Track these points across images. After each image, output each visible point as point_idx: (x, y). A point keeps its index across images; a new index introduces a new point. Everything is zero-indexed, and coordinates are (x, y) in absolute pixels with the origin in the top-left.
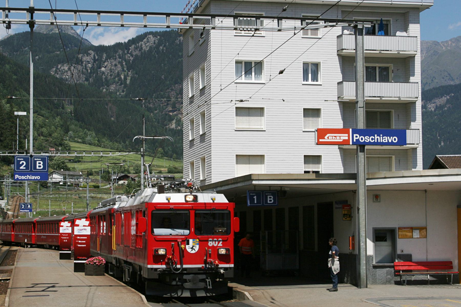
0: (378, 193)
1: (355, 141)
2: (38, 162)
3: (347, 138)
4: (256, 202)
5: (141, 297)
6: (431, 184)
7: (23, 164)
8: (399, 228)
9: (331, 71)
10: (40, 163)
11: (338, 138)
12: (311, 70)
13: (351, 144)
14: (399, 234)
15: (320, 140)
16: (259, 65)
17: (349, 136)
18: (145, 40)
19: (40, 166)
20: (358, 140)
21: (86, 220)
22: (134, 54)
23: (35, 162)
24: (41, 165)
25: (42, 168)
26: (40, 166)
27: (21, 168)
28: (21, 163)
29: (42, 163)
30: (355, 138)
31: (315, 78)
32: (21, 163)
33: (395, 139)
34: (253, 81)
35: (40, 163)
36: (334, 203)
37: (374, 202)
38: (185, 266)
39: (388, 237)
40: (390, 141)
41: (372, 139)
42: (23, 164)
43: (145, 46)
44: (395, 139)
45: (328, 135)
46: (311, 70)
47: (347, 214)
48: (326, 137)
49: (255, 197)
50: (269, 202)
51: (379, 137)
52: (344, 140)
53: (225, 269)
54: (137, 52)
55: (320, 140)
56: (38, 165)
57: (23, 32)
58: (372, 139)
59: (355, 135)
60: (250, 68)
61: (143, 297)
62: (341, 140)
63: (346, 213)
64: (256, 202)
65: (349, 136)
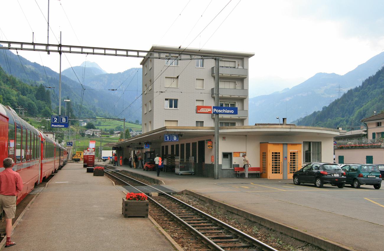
0: (225, 136)
1: (214, 112)
2: (63, 119)
3: (210, 110)
7: (56, 119)
8: (234, 152)
23: (62, 119)
24: (65, 120)
26: (64, 121)
27: (55, 121)
28: (55, 119)
29: (65, 119)
30: (214, 111)
32: (55, 119)
33: (232, 112)
35: (64, 119)
37: (223, 140)
39: (229, 156)
40: (230, 112)
42: (56, 119)
44: (232, 112)
45: (202, 109)
47: (210, 146)
48: (201, 110)
49: (168, 137)
51: (225, 110)
56: (63, 120)
58: (222, 111)
59: (214, 109)
63: (210, 145)
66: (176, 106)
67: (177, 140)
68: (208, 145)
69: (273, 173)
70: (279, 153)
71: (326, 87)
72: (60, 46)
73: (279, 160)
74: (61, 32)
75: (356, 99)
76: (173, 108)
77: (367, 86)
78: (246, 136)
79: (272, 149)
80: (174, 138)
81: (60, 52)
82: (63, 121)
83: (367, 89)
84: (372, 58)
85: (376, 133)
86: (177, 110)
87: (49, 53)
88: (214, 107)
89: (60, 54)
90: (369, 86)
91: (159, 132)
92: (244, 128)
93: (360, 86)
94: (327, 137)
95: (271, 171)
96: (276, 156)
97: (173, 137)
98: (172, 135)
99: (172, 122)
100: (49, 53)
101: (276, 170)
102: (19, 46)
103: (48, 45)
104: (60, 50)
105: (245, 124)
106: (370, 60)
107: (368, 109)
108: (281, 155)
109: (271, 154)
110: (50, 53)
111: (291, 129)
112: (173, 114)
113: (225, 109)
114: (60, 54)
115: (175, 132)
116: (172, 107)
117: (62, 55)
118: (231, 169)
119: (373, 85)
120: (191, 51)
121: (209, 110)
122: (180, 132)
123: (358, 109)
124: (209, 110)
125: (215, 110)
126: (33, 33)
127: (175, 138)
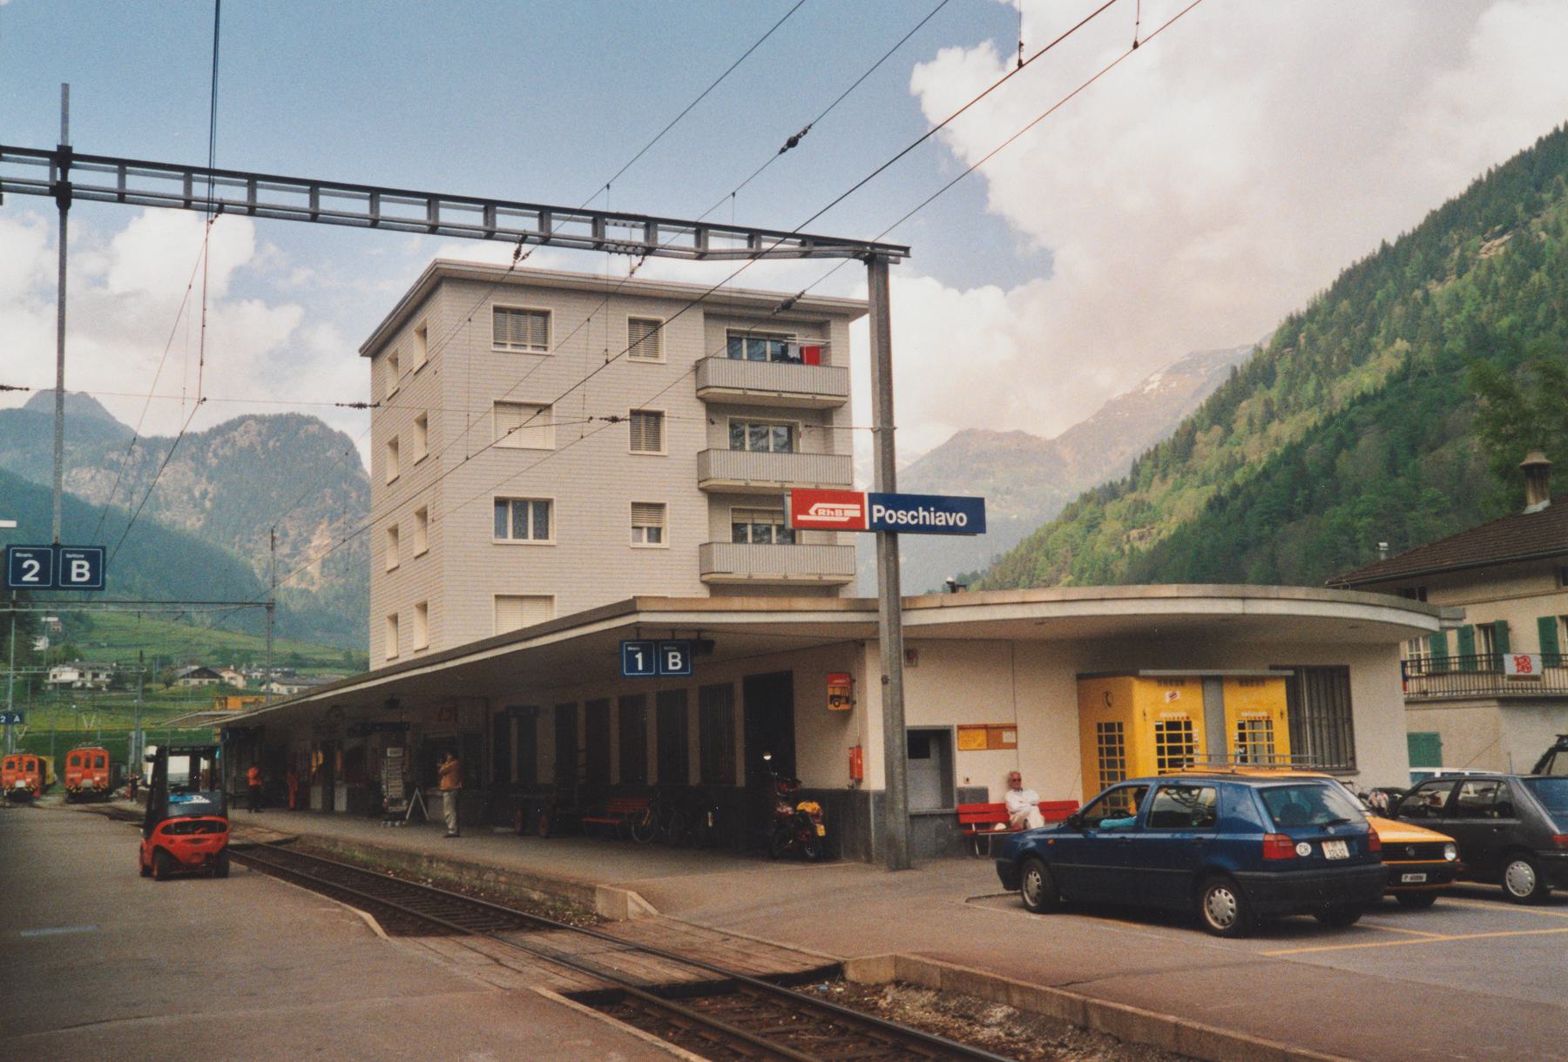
2: (75, 563)
3: (857, 514)
4: (640, 667)
5: (361, 918)
6: (1042, 622)
7: (31, 567)
8: (961, 728)
9: (687, 431)
10: (80, 567)
11: (838, 512)
12: (647, 423)
13: (867, 526)
14: (957, 740)
15: (801, 517)
16: (548, 407)
17: (862, 510)
18: (242, 428)
19: (80, 575)
20: (881, 519)
21: (1557, 130)
22: (221, 452)
23: (68, 564)
24: (85, 571)
25: (87, 577)
26: (80, 575)
27: (27, 578)
28: (25, 565)
29: (87, 565)
30: (876, 515)
32: (25, 565)
35: (80, 567)
39: (934, 751)
41: (913, 518)
42: (31, 567)
43: (242, 439)
45: (817, 506)
46: (647, 423)
47: (839, 697)
48: (812, 511)
49: (639, 656)
50: (671, 667)
52: (853, 519)
53: (1492, 817)
54: (227, 451)
55: (801, 517)
56: (75, 571)
58: (913, 518)
59: (875, 507)
61: (367, 916)
62: (845, 519)
63: (838, 692)
64: (640, 667)
65: (862, 510)
66: (542, 532)
67: (684, 668)
68: (830, 692)
70: (1188, 725)
72: (63, 158)
74: (65, 87)
76: (531, 540)
80: (671, 661)
81: (63, 194)
85: (1480, 626)
86: (550, 550)
88: (874, 499)
89: (64, 206)
92: (942, 607)
93: (1124, 481)
94: (1377, 644)
98: (657, 642)
99: (527, 605)
104: (59, 178)
108: (1197, 731)
109: (1153, 733)
111: (1248, 602)
112: (525, 564)
113: (926, 509)
114: (64, 206)
115: (673, 628)
116: (525, 536)
117: (70, 211)
118: (948, 811)
120: (640, 292)
121: (852, 511)
122: (699, 629)
124: (852, 511)
125: (879, 511)
127: (675, 662)
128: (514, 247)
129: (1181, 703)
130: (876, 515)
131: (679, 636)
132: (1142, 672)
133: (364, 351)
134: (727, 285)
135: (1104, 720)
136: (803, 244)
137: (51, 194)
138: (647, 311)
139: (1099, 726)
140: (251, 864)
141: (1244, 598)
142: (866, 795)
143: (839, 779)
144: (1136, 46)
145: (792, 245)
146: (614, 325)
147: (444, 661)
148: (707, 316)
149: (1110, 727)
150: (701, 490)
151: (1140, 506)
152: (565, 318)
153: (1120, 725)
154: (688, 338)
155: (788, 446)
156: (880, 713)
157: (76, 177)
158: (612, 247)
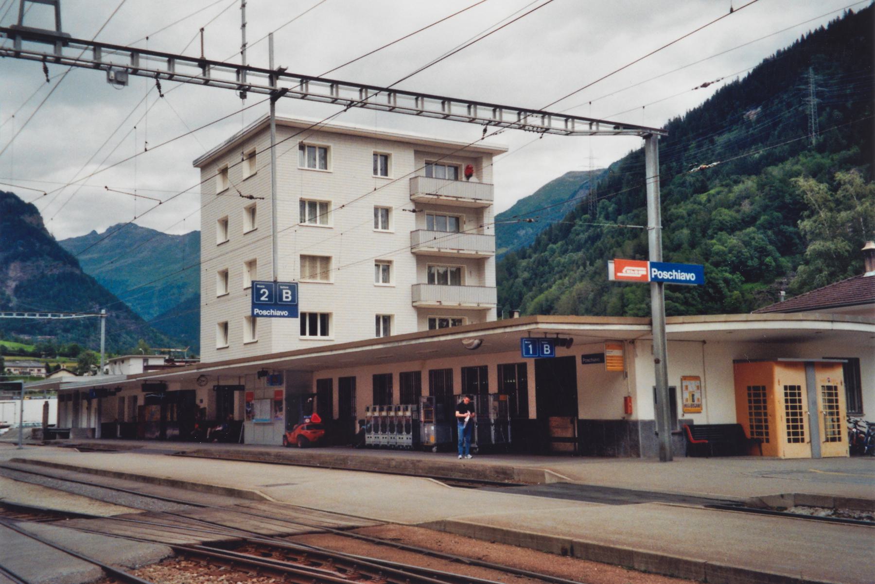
2: (284, 291)
3: (644, 273)
6: (730, 332)
7: (264, 293)
15: (619, 274)
20: (656, 276)
24: (289, 295)
25: (290, 299)
26: (287, 297)
27: (263, 298)
28: (262, 292)
29: (290, 292)
30: (653, 274)
31: (386, 225)
32: (262, 292)
34: (318, 224)
36: (579, 360)
38: (493, 428)
42: (264, 293)
48: (624, 271)
49: (530, 346)
57: (749, 75)
59: (653, 270)
60: (314, 208)
69: (789, 441)
71: (145, 268)
73: (800, 408)
75: (526, 275)
77: (548, 245)
78: (704, 342)
79: (783, 378)
82: (284, 299)
83: (547, 253)
84: (544, 188)
87: (243, 96)
90: (551, 246)
91: (413, 342)
95: (786, 437)
96: (792, 392)
97: (542, 345)
98: (538, 339)
100: (243, 96)
101: (795, 436)
102: (162, 66)
103: (242, 70)
105: (463, 324)
106: (539, 191)
107: (558, 298)
109: (783, 391)
110: (248, 94)
119: (560, 243)
123: (533, 298)
126: (202, 30)
127: (547, 350)
128: (484, 127)
129: (796, 378)
130: (653, 274)
131: (548, 336)
132: (780, 359)
133: (196, 164)
134: (325, 122)
135: (751, 384)
136: (615, 128)
137: (238, 89)
138: (382, 149)
139: (749, 388)
140: (212, 454)
141: (832, 321)
142: (636, 423)
143: (613, 412)
144: (732, 11)
145: (610, 128)
146: (365, 156)
147: (372, 345)
148: (417, 152)
149: (756, 388)
150: (413, 253)
151: (543, 262)
152: (338, 152)
153: (764, 388)
154: (403, 164)
155: (458, 229)
156: (534, 379)
157: (281, 84)
158: (531, 128)
